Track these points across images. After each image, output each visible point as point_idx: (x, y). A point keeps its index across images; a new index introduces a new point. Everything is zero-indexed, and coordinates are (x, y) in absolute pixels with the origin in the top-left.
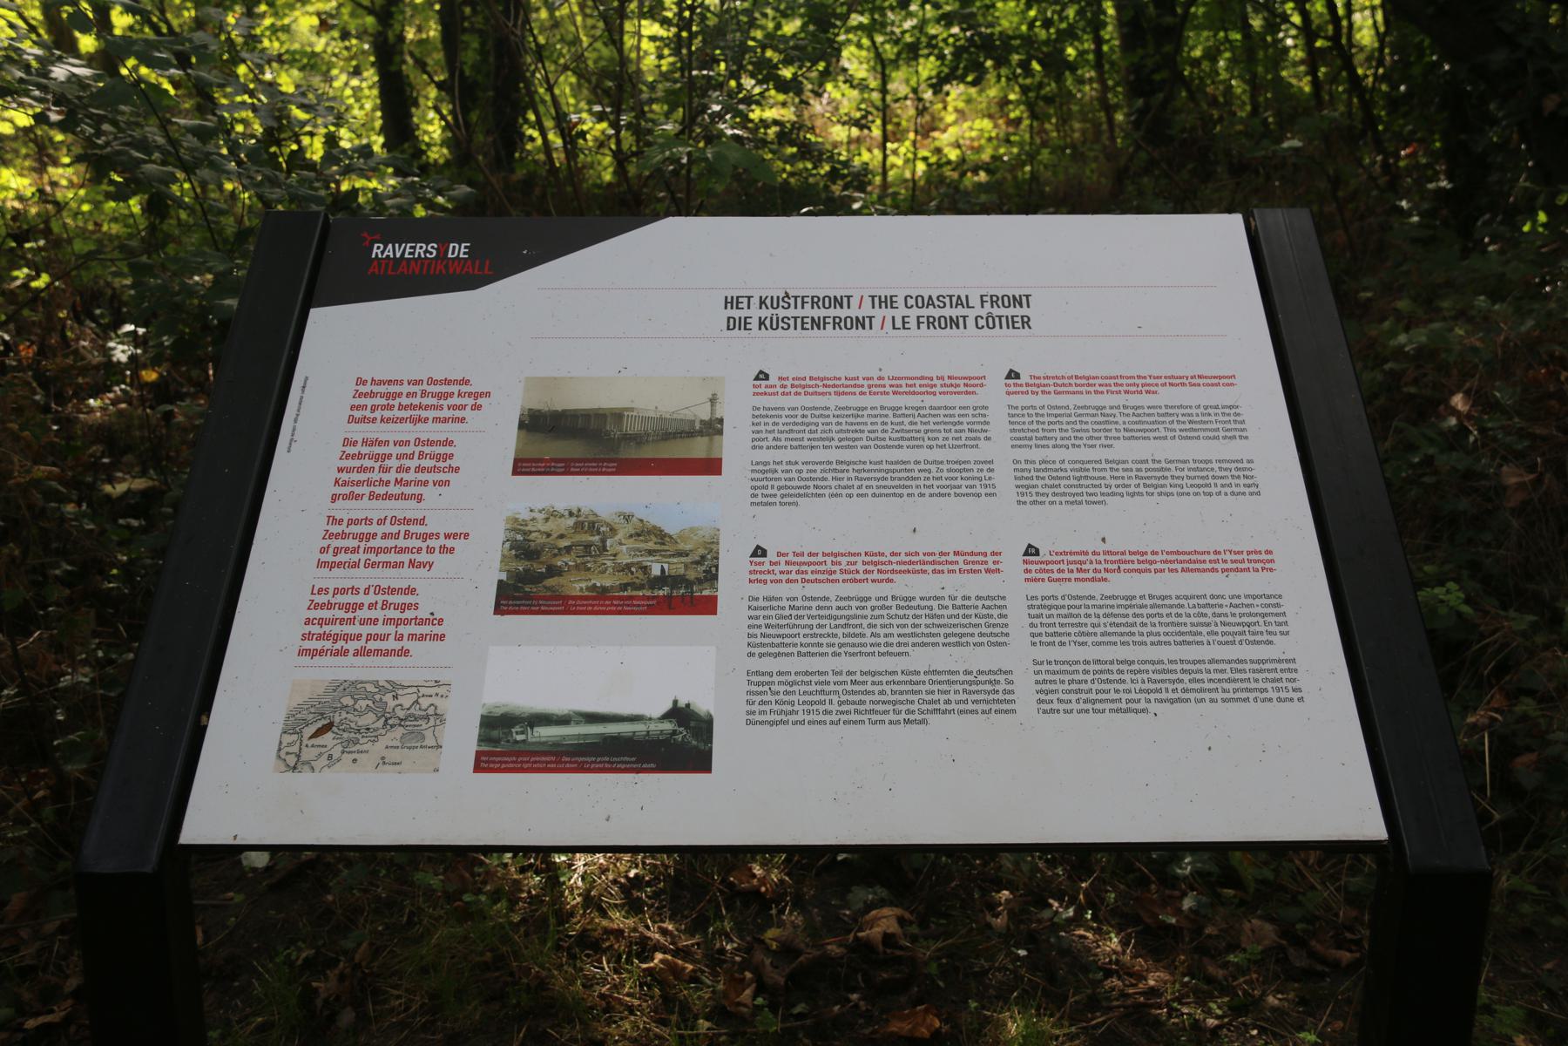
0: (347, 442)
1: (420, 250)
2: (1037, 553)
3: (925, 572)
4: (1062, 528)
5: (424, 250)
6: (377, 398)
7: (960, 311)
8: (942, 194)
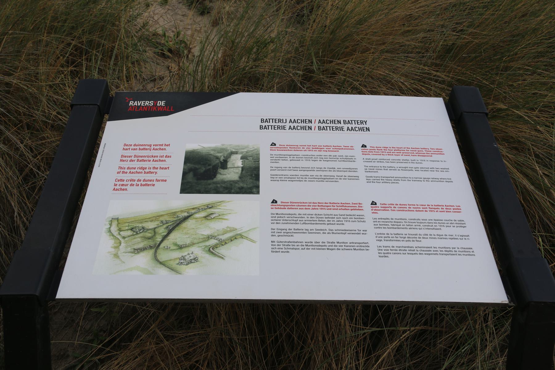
1: (147, 103)
5: (149, 103)
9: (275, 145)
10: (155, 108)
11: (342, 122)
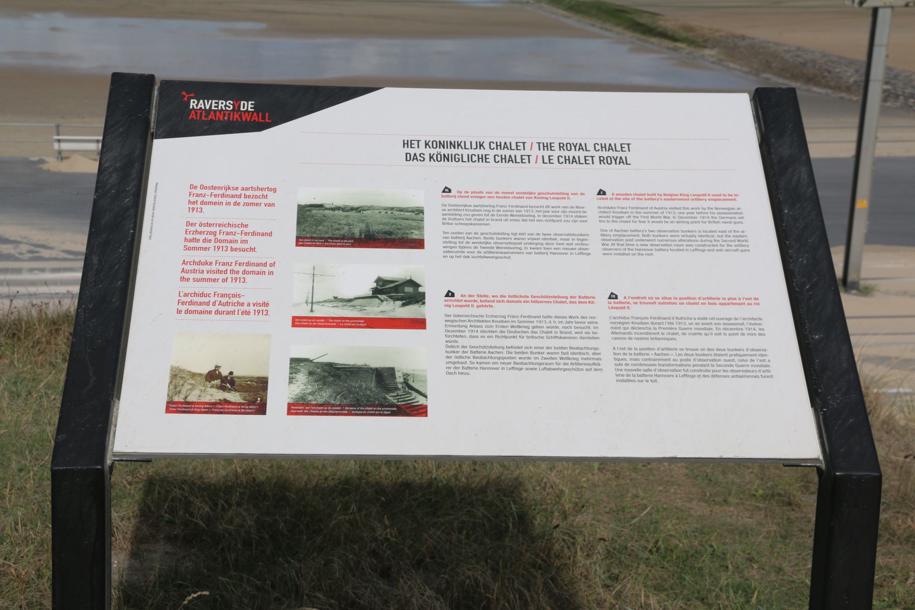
1: (222, 104)
2: (616, 298)
3: (701, 334)
4: (636, 275)
6: (200, 197)
8: (712, 62)
10: (236, 116)
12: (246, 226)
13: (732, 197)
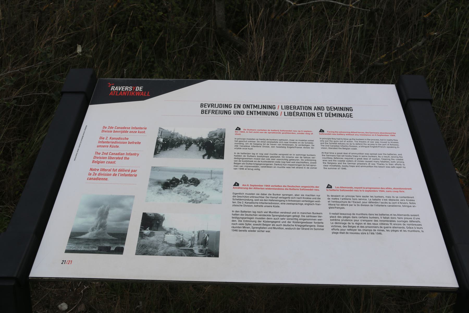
0: (101, 138)
1: (127, 88)
2: (331, 187)
4: (339, 178)
7: (228, 109)
9: (240, 129)
10: (133, 93)
11: (313, 108)
12: (128, 139)
13: (393, 134)
